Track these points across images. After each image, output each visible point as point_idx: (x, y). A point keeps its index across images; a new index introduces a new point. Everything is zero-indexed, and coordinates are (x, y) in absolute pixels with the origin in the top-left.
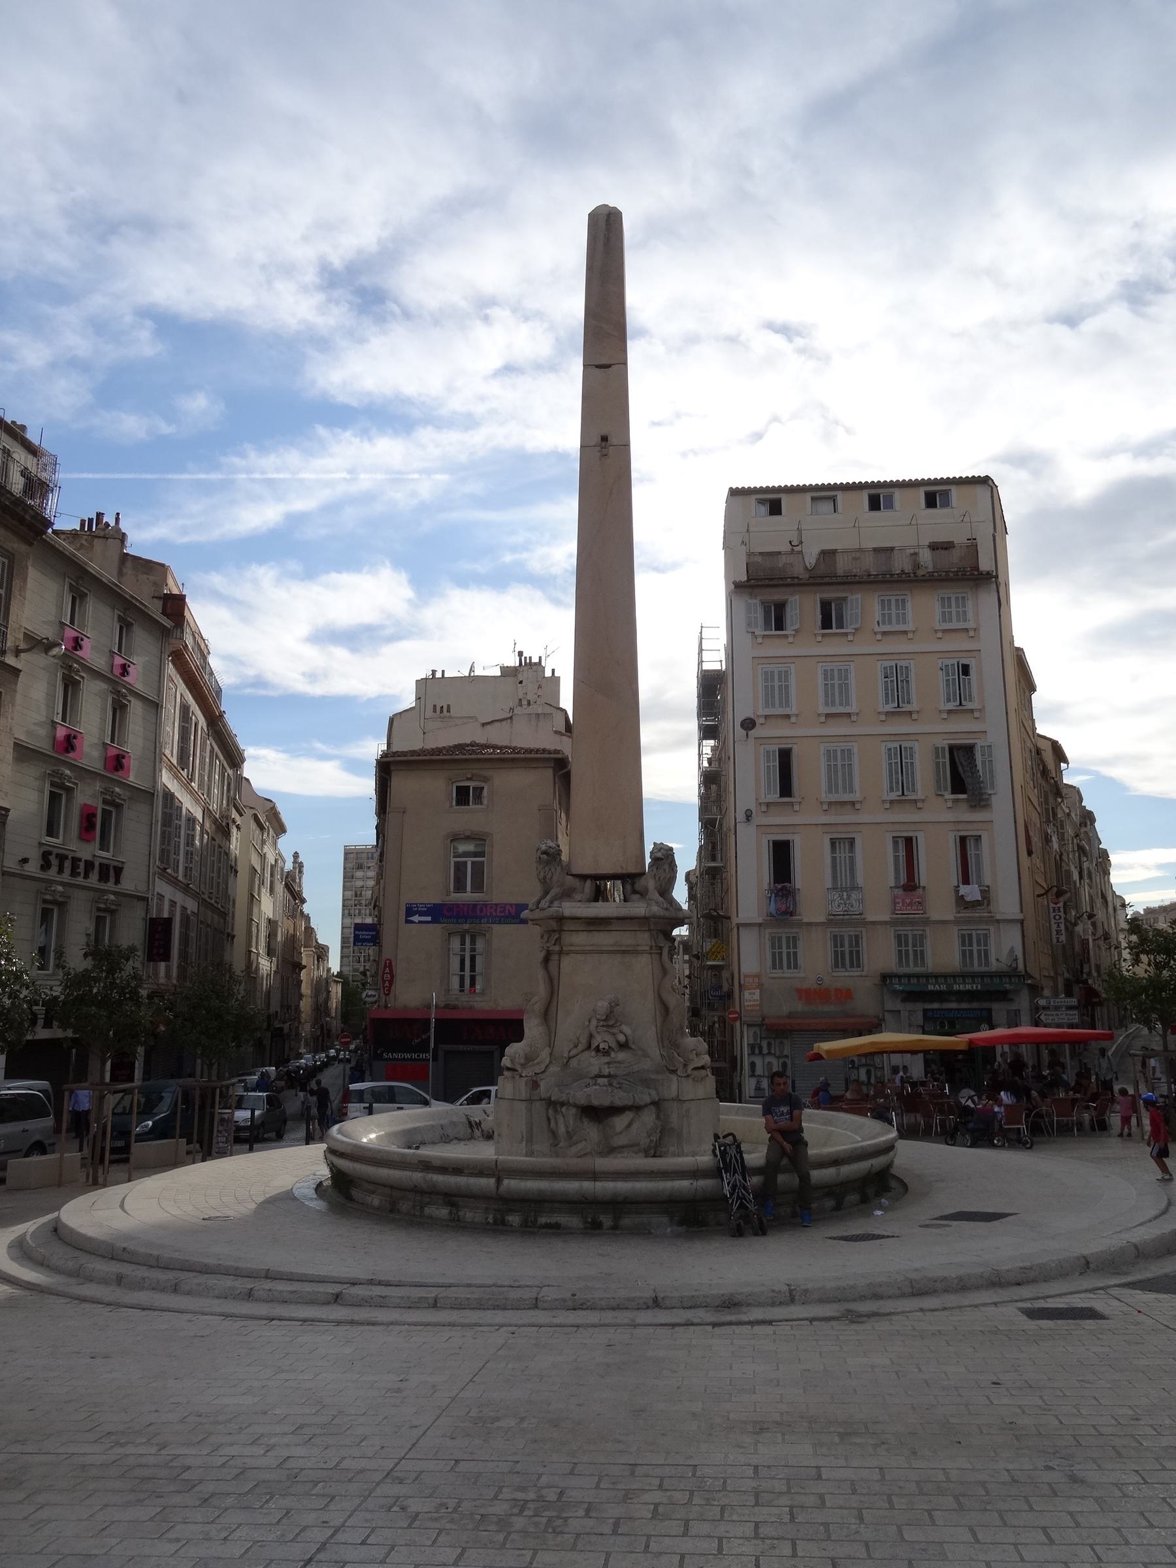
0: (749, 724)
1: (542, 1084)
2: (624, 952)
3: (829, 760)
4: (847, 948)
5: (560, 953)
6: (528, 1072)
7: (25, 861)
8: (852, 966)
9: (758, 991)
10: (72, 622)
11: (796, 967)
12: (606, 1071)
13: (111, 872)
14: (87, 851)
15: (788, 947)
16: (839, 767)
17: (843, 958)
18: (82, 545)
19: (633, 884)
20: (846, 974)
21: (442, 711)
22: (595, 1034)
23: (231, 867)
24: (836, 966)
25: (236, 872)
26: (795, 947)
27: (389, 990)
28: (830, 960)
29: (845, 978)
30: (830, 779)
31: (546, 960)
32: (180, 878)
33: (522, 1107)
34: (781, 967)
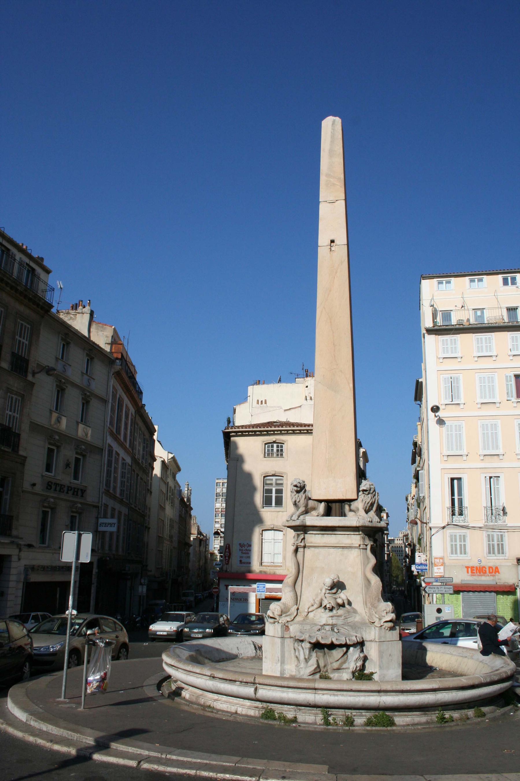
0: (435, 409)
1: (291, 628)
2: (343, 547)
3: (483, 430)
4: (496, 543)
5: (305, 547)
6: (284, 619)
7: (34, 485)
8: (499, 553)
9: (442, 567)
10: (62, 358)
11: (465, 553)
12: (330, 622)
13: (82, 492)
14: (66, 479)
15: (460, 541)
16: (490, 434)
17: (493, 549)
18: (71, 317)
19: (350, 506)
20: (495, 558)
21: (262, 403)
22: (324, 598)
23: (148, 490)
24: (490, 553)
25: (151, 493)
26: (464, 541)
27: (228, 561)
28: (486, 550)
29: (492, 561)
30: (484, 442)
31: (296, 551)
32: (118, 495)
33: (279, 641)
34: (456, 553)
